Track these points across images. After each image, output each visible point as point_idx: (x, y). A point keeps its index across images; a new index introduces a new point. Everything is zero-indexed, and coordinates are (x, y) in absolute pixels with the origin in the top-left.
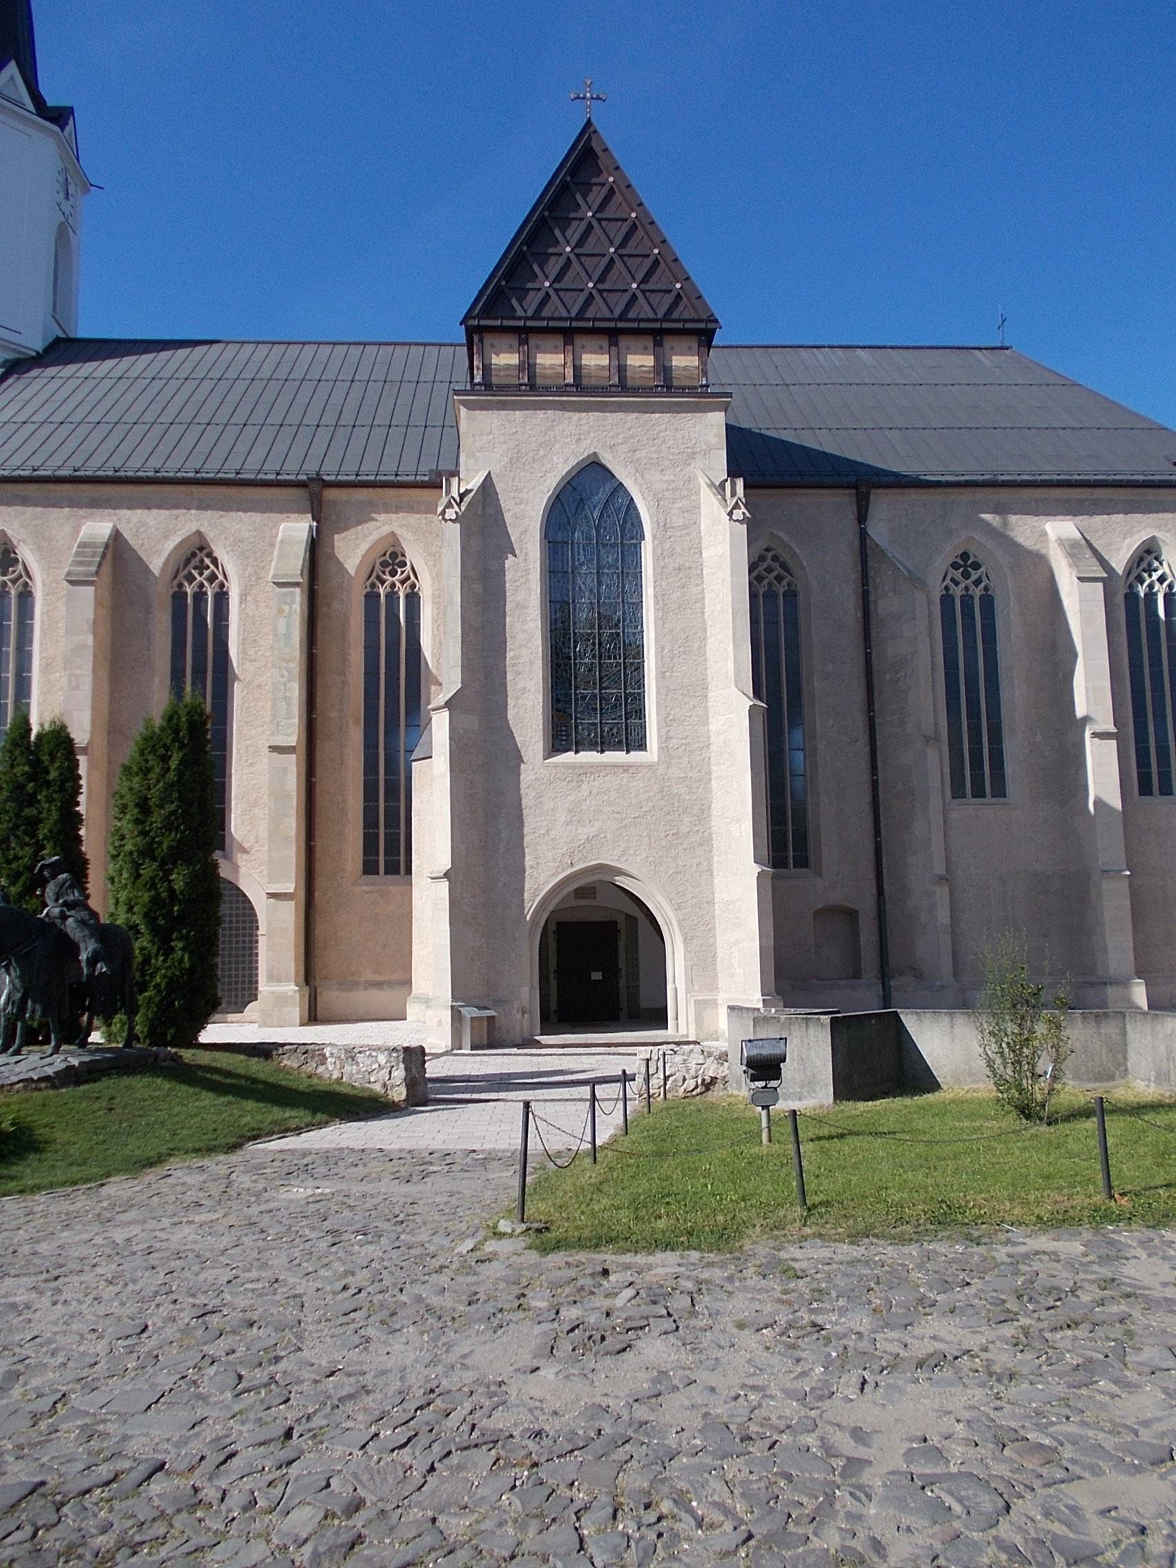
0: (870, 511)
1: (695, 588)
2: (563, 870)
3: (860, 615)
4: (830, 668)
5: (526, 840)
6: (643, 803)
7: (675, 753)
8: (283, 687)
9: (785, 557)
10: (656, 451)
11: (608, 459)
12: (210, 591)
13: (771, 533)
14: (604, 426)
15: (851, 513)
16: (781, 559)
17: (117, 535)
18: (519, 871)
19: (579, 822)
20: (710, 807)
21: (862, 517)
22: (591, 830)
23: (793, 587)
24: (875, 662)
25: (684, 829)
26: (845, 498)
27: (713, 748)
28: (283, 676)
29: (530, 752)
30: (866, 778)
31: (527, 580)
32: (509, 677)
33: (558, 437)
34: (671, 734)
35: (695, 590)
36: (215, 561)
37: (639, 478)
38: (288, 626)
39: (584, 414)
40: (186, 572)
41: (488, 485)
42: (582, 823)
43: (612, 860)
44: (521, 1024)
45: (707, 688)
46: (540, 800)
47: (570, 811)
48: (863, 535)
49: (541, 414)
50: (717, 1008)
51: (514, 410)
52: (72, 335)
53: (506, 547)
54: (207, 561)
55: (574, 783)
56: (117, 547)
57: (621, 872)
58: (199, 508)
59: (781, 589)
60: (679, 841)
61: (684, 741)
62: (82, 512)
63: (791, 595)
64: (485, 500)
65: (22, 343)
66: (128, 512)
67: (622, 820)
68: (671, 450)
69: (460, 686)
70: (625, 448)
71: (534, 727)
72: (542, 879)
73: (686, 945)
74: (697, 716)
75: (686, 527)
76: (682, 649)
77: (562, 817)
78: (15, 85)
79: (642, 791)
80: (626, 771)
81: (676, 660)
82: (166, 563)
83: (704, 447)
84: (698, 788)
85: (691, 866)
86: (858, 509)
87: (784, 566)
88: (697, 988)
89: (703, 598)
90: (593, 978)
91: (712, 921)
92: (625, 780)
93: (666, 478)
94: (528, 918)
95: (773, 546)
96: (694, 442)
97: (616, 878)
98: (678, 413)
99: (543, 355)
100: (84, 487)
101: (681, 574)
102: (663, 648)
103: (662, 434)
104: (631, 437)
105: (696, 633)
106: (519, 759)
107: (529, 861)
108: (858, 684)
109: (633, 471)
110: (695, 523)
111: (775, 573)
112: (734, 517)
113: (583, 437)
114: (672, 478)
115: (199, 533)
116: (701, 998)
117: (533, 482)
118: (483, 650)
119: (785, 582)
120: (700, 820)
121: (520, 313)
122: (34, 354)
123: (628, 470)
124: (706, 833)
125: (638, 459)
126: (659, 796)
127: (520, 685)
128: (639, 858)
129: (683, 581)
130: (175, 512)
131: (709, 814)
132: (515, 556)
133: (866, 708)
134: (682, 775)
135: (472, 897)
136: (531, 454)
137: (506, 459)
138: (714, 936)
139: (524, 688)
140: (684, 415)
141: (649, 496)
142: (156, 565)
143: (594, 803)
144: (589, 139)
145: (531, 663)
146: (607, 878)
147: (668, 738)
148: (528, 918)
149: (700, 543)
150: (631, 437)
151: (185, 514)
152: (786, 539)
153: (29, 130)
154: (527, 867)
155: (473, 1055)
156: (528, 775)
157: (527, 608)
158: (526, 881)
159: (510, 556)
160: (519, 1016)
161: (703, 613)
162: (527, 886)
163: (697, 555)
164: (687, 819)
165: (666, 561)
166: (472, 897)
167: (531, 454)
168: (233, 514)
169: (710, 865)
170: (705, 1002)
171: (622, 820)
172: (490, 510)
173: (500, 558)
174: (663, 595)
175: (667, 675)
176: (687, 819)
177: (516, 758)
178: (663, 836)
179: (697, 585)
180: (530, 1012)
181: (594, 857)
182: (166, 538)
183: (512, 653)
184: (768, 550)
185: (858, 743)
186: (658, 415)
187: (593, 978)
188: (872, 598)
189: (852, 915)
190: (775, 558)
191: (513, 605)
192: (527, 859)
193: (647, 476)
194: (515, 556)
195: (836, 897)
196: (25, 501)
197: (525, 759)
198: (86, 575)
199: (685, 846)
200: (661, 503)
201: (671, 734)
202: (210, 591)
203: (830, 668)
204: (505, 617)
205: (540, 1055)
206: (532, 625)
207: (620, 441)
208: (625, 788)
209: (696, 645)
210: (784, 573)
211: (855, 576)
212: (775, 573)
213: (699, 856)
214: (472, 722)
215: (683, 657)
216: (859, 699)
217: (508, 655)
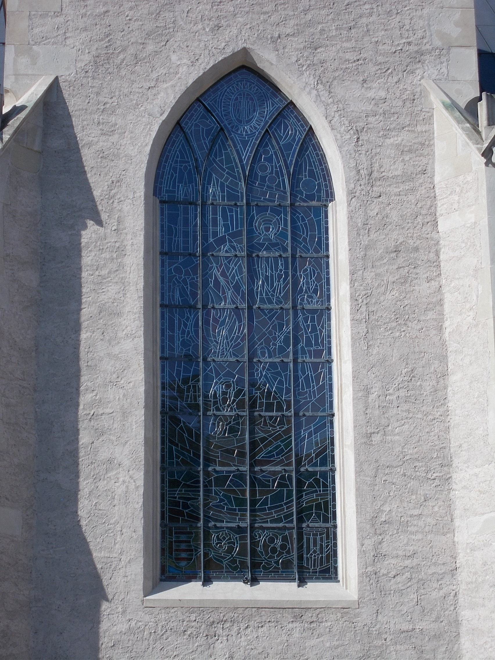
32: (84, 438)
34: (385, 548)
37: (324, 94)
45: (450, 465)
55: (201, 640)
61: (407, 562)
75: (408, 178)
76: (402, 393)
81: (392, 412)
83: (438, 43)
92: (296, 635)
93: (371, 94)
103: (364, 20)
109: (312, 81)
110: (424, 172)
123: (304, 79)
134: (405, 626)
137: (87, 58)
145: (125, 414)
157: (119, 314)
161: (440, 329)
165: (373, 236)
167: (132, 50)
197: (110, 591)
200: (364, 137)
207: (289, 31)
215: (406, 407)
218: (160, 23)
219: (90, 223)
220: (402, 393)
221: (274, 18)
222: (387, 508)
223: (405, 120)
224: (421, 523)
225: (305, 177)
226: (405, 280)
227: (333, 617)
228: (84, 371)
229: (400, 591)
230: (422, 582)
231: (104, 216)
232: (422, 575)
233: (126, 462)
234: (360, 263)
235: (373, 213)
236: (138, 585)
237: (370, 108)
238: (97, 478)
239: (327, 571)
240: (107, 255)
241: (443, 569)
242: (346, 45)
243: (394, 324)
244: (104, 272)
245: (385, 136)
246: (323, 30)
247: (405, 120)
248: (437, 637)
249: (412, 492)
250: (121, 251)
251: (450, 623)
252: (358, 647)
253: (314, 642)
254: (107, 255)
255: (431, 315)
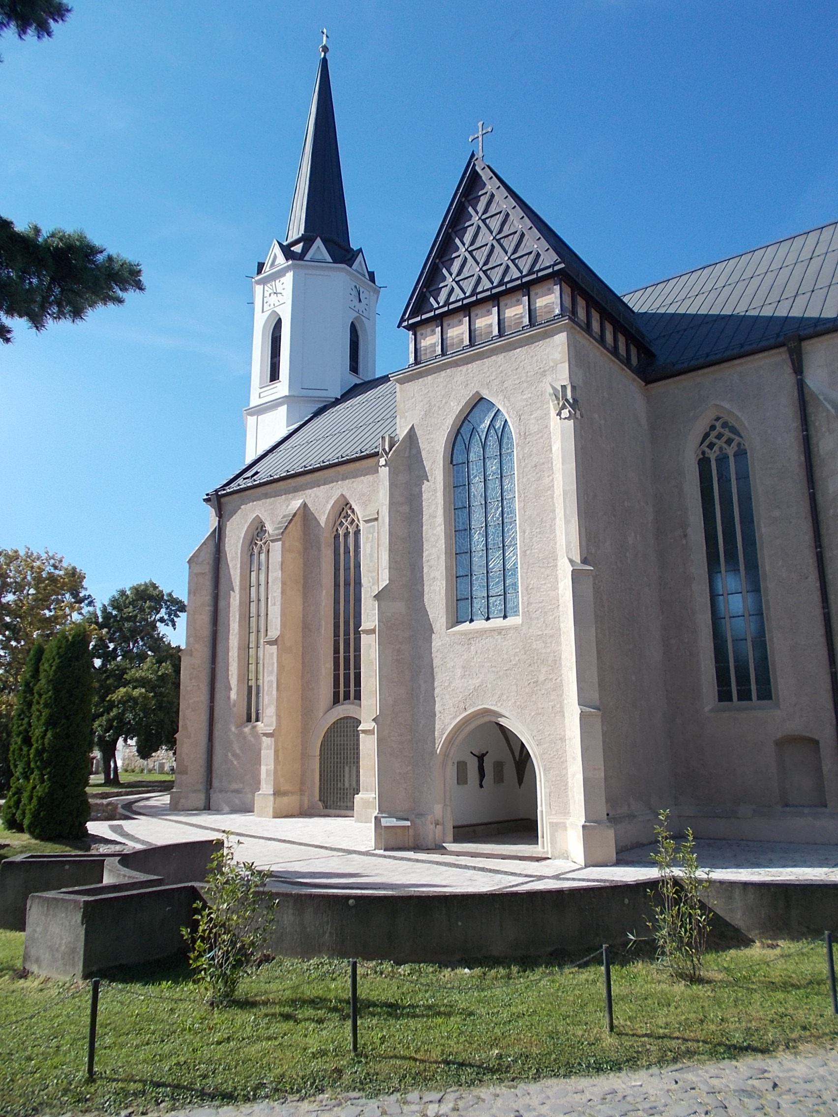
0: (804, 363)
1: (547, 479)
2: (460, 714)
3: (803, 458)
4: (776, 513)
5: (437, 691)
6: (512, 658)
7: (534, 616)
8: (369, 589)
9: (732, 422)
10: (518, 378)
11: (485, 394)
12: (351, 530)
13: (716, 405)
14: (483, 369)
15: (788, 370)
16: (730, 425)
17: (305, 505)
18: (431, 716)
19: (469, 675)
20: (560, 658)
21: (798, 369)
22: (476, 682)
23: (742, 447)
24: (820, 499)
25: (542, 678)
26: (779, 358)
27: (561, 608)
28: (370, 582)
29: (438, 625)
30: (818, 612)
31: (436, 496)
32: (425, 570)
33: (454, 387)
34: (531, 600)
35: (546, 480)
36: (353, 511)
37: (506, 402)
38: (372, 548)
39: (470, 365)
40: (339, 521)
41: (412, 435)
42: (471, 676)
43: (492, 705)
44: (434, 832)
45: (557, 559)
46: (445, 660)
47: (464, 667)
48: (801, 385)
49: (443, 374)
50: (566, 830)
51: (427, 376)
52: (367, 380)
53: (423, 476)
54: (349, 512)
55: (466, 646)
56: (305, 514)
57: (502, 716)
58: (343, 480)
59: (731, 451)
60: (539, 688)
61: (540, 605)
62: (290, 496)
63: (741, 454)
64: (411, 444)
65: (329, 396)
66: (310, 491)
67: (497, 672)
68: (529, 374)
69: (388, 582)
70: (496, 382)
71: (440, 605)
72: (447, 721)
73: (545, 774)
74: (549, 583)
75: (540, 431)
76: (538, 530)
77: (459, 672)
78: (321, 252)
79: (511, 648)
80: (500, 633)
81: (534, 539)
82: (328, 518)
83: (552, 364)
84: (551, 642)
85: (548, 708)
86: (793, 363)
87: (733, 430)
88: (554, 812)
89: (553, 486)
90: (436, 806)
91: (565, 754)
92: (499, 641)
93: (525, 397)
94: (438, 752)
95: (721, 415)
96: (544, 362)
97: (499, 719)
98: (532, 343)
99: (452, 330)
100: (289, 481)
101: (537, 470)
102: (524, 532)
103: (522, 363)
104: (501, 372)
105: (548, 515)
106: (431, 631)
107: (438, 707)
108: (806, 526)
109: (502, 398)
110: (546, 427)
111: (724, 439)
112: (563, 416)
113: (469, 382)
114: (529, 395)
115: (342, 495)
116: (555, 821)
117: (439, 425)
118: (409, 553)
119: (734, 444)
120: (553, 670)
121: (436, 306)
122: (334, 400)
123: (499, 398)
124: (558, 681)
125: (506, 388)
126: (523, 652)
127: (432, 576)
128: (510, 703)
129: (538, 475)
130: (331, 485)
131: (560, 664)
132: (428, 481)
133: (813, 544)
134: (540, 633)
135: (398, 736)
136: (437, 405)
137: (423, 413)
138: (566, 768)
139: (434, 578)
140: (537, 344)
141: (513, 414)
142: (322, 520)
143: (479, 660)
144: (474, 165)
145: (438, 558)
146: (494, 719)
147: (529, 604)
148: (438, 752)
149: (550, 442)
150: (501, 372)
151: (335, 485)
152: (727, 406)
153: (326, 273)
154: (437, 713)
155: (385, 857)
156: (437, 642)
157: (435, 517)
158: (437, 722)
159: (425, 481)
160: (432, 827)
161: (553, 498)
162: (437, 727)
163: (549, 452)
164: (545, 669)
165: (526, 461)
166: (398, 736)
167: (437, 405)
168: (359, 479)
169: (562, 707)
170: (557, 824)
171: (497, 672)
172: (414, 452)
173: (419, 485)
174: (524, 489)
175: (528, 552)
176: (545, 669)
177: (429, 630)
178: (526, 684)
179: (548, 477)
180: (443, 824)
181: (480, 703)
182: (327, 502)
183: (427, 552)
184: (718, 419)
185: (809, 579)
186: (518, 350)
187: (436, 806)
188: (814, 441)
189: (814, 743)
190: (725, 425)
191: (428, 516)
192: (437, 706)
193: (512, 399)
194: (428, 481)
195: (796, 726)
196: (266, 496)
197: (435, 631)
198: (277, 535)
199: (543, 691)
200: (522, 418)
201: (531, 600)
202: (351, 530)
203: (776, 513)
204: (422, 527)
205: (417, 861)
206: (439, 529)
207: (493, 378)
208: (499, 647)
209: (548, 525)
210: (732, 436)
211: (795, 424)
212: (724, 439)
213: (554, 700)
214: (399, 607)
215: (539, 536)
216: (807, 537)
217: (425, 554)
218: (447, 390)
219: (425, 482)
220: (538, 530)
221: (488, 374)
222: (532, 582)
223: (539, 405)
224: (545, 587)
225: (505, 441)
226: (539, 479)
227: (512, 632)
228: (425, 543)
229: (537, 618)
230: (546, 613)
231: (429, 478)
232: (546, 610)
233: (439, 578)
234: (521, 475)
235: (526, 451)
236: (444, 627)
237: (524, 403)
238: (430, 586)
239: (516, 612)
240: (431, 493)
241: (554, 606)
242: (516, 377)
243: (534, 500)
244: (430, 501)
245: (531, 415)
246: (506, 374)
247: (539, 405)
248: (552, 636)
249: (542, 573)
250: (435, 491)
251: (557, 630)
252: (521, 644)
253: (506, 643)
254: (431, 493)
255: (549, 492)
